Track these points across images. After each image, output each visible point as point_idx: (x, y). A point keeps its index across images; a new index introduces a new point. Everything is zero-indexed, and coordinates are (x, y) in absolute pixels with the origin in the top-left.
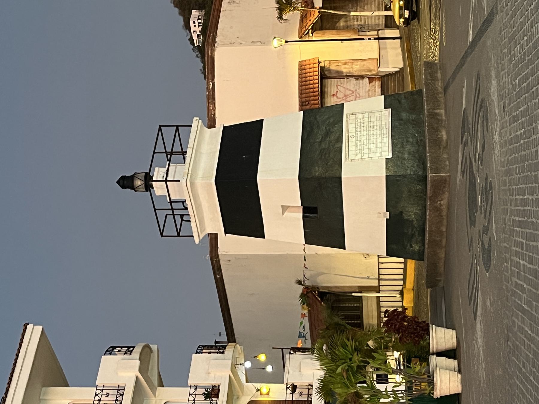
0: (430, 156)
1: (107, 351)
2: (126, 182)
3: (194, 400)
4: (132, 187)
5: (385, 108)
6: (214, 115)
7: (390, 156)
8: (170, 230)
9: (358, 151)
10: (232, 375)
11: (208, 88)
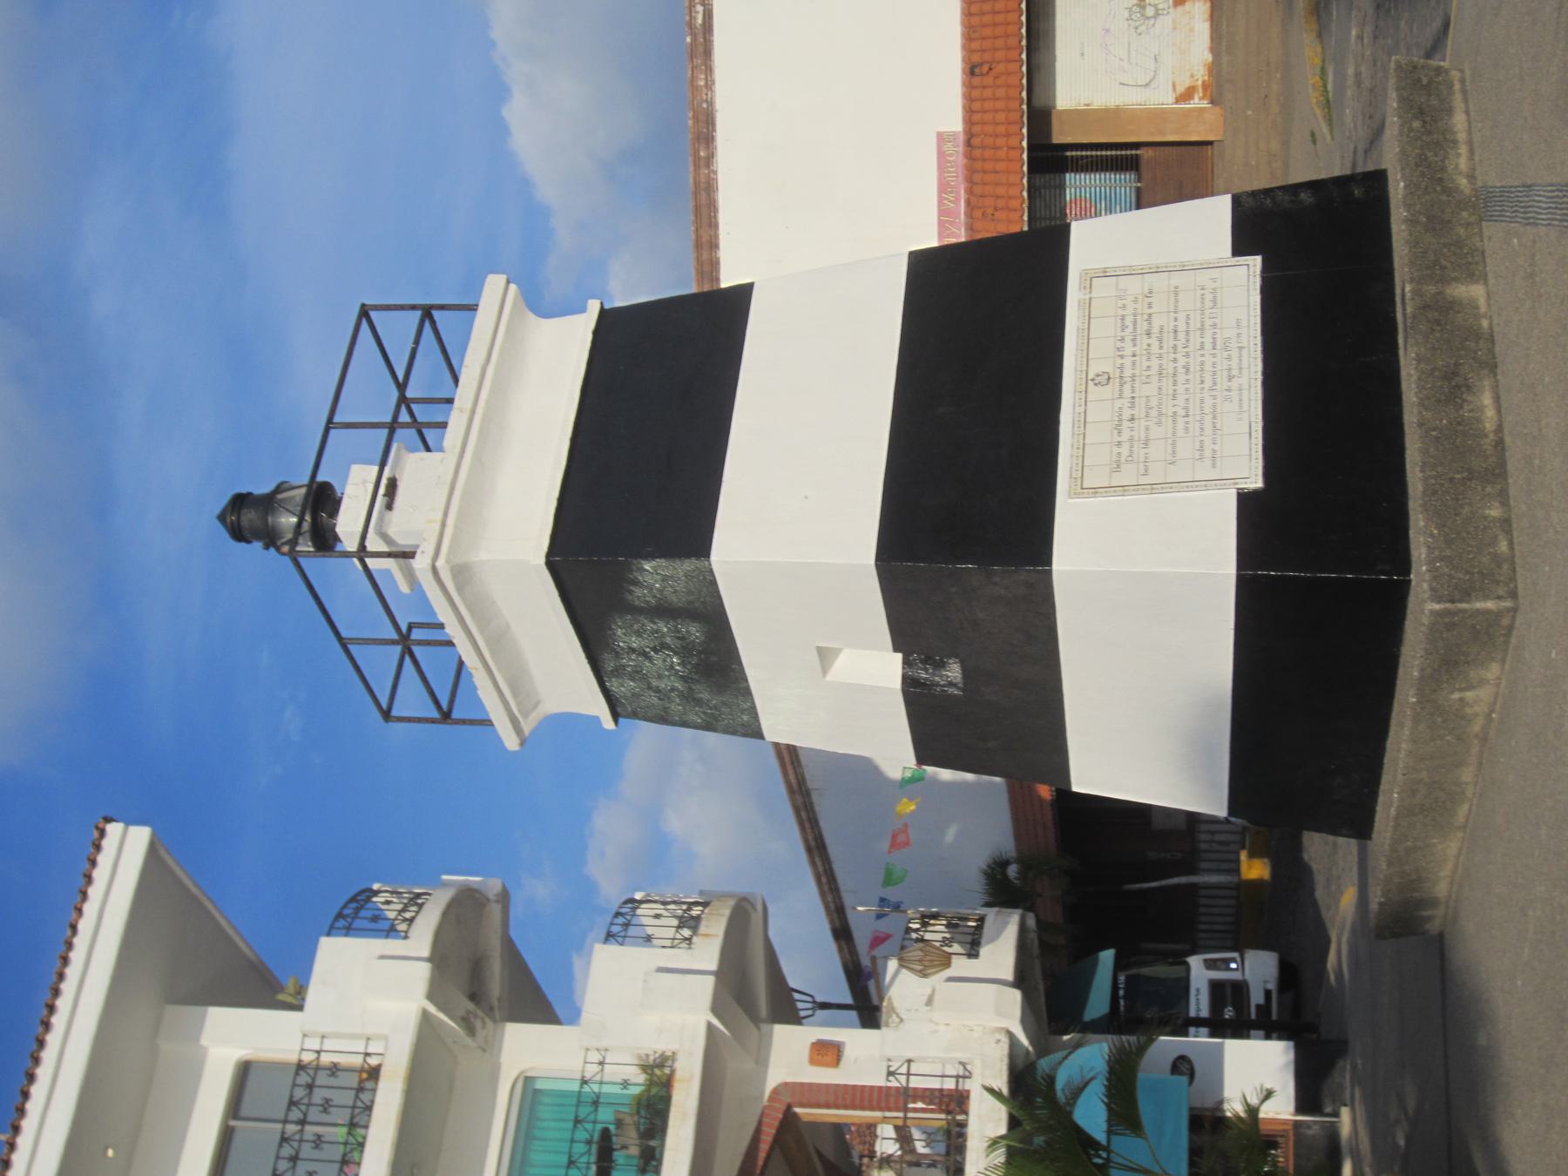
1: (340, 916)
2: (246, 517)
4: (270, 538)
6: (711, 103)
7: (1257, 483)
9: (1125, 450)
11: (691, 25)
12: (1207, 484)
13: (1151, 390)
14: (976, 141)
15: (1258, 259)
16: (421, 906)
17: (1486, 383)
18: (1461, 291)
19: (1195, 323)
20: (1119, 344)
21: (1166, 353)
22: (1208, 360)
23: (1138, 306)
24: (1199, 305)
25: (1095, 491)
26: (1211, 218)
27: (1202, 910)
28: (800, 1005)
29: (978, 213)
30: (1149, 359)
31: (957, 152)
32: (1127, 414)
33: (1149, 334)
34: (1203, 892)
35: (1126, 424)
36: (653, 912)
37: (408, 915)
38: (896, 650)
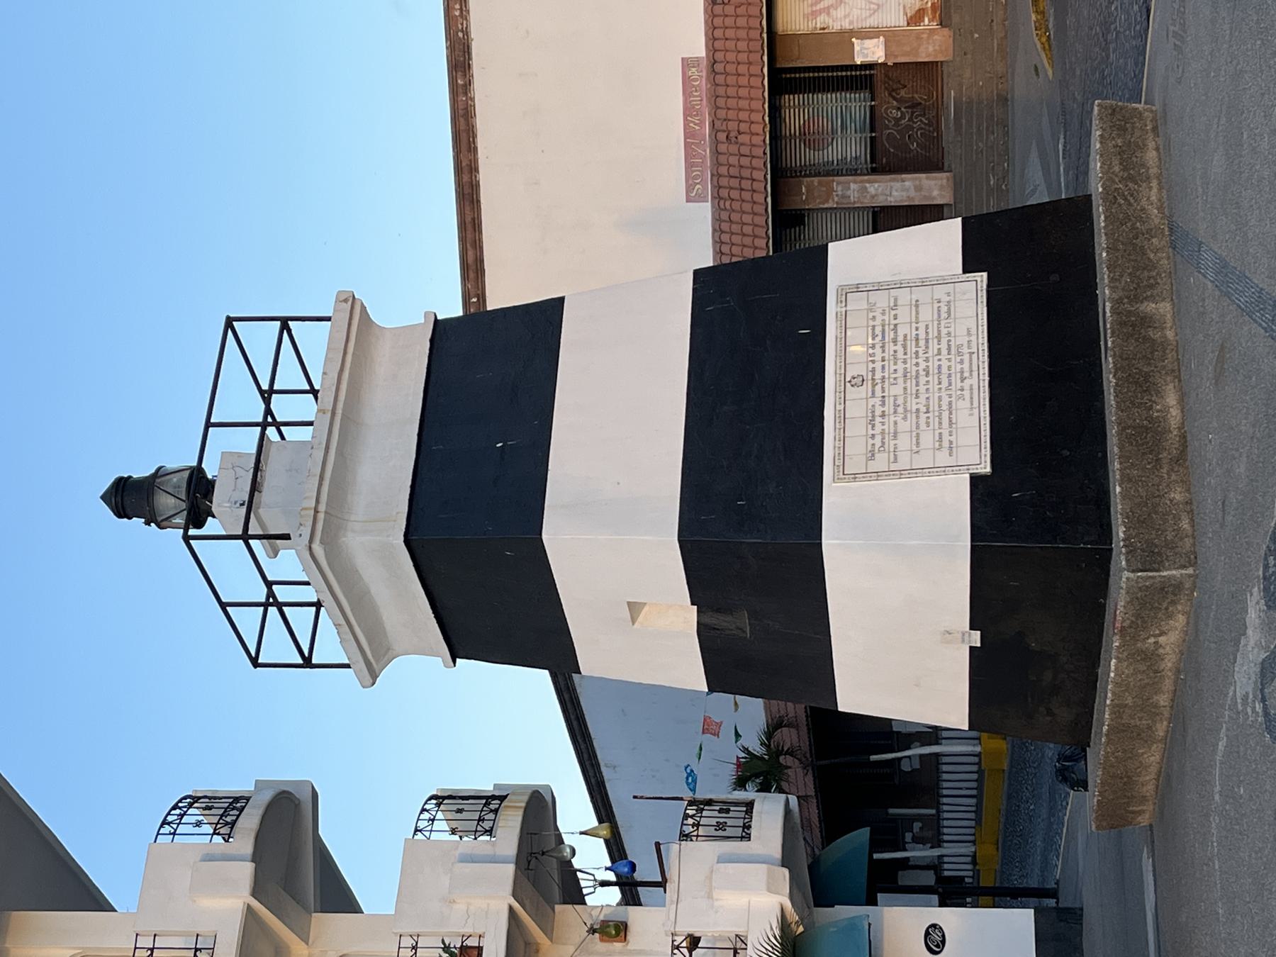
0: (1124, 495)
1: (164, 823)
2: (128, 498)
3: (415, 948)
5: (965, 271)
6: (466, 32)
7: (986, 468)
8: (278, 647)
10: (516, 905)
12: (945, 470)
13: (897, 390)
14: (719, 67)
15: (985, 274)
16: (241, 810)
17: (1171, 386)
18: (1149, 307)
19: (933, 333)
20: (871, 351)
21: (906, 314)
22: (945, 364)
23: (886, 317)
24: (936, 316)
25: (855, 477)
26: (947, 236)
27: (945, 776)
28: (583, 884)
29: (722, 136)
30: (895, 364)
31: (700, 77)
32: (878, 412)
33: (895, 342)
34: (945, 759)
35: (878, 419)
36: (455, 807)
37: (229, 819)
38: (693, 604)
